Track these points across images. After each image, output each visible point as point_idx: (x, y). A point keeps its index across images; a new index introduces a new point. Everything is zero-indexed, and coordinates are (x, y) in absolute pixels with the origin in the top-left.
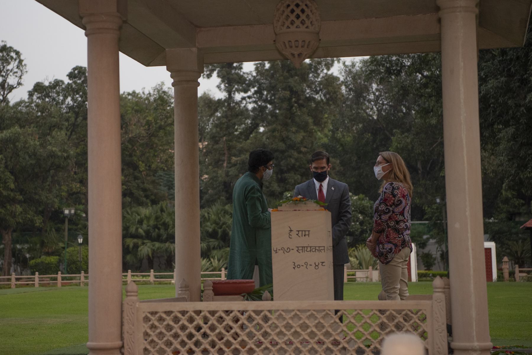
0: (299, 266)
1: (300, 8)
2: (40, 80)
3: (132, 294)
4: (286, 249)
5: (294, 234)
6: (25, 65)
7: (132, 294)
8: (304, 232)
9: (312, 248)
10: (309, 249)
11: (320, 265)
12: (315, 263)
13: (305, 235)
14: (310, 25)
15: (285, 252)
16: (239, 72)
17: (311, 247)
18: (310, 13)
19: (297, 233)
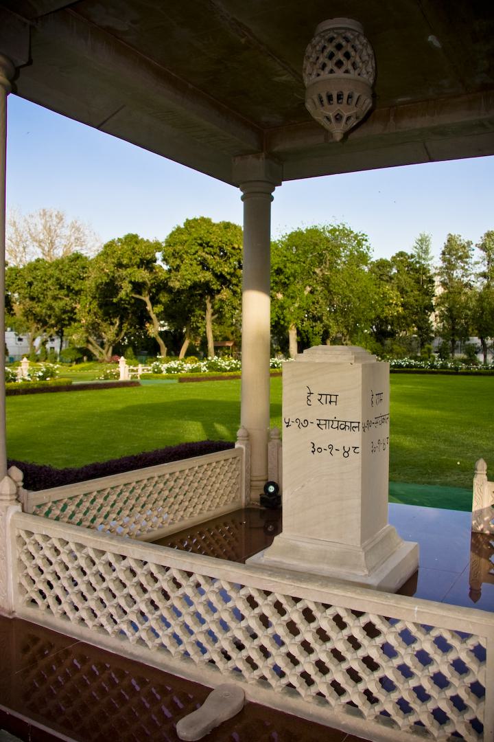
1: (343, 51)
2: (139, 235)
4: (302, 421)
5: (314, 398)
6: (421, 235)
8: (328, 397)
9: (340, 423)
10: (335, 425)
11: (351, 452)
13: (330, 402)
14: (350, 67)
17: (338, 421)
18: (358, 59)
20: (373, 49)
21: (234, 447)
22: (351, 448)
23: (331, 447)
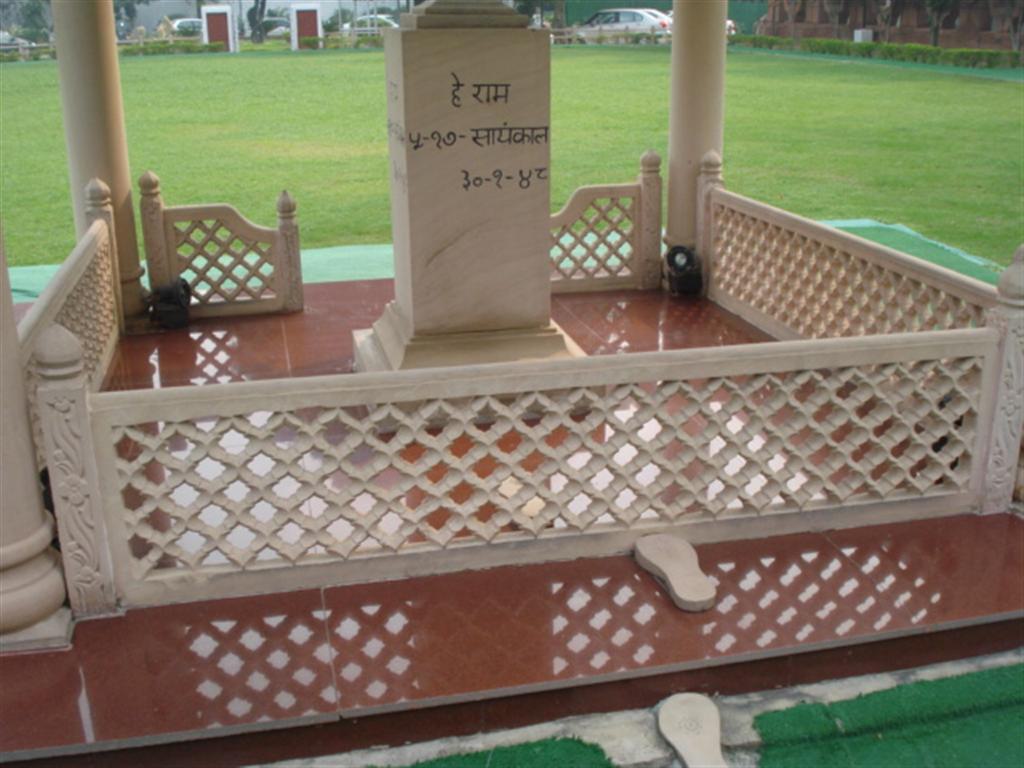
11: (534, 179)
15: (442, 144)
19: (475, 90)
22: (533, 171)
23: (498, 174)
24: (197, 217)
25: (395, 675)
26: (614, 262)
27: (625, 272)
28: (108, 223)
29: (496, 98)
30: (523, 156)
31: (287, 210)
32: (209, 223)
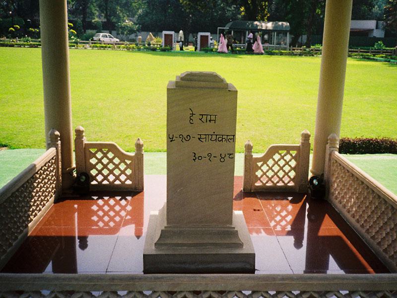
0: (200, 158)
3: (203, 84)
5: (196, 118)
7: (203, 84)
10: (214, 137)
11: (227, 158)
12: (221, 155)
16: (125, 23)
17: (217, 135)
19: (201, 117)
20: (264, 30)
21: (254, 273)
22: (226, 154)
23: (210, 155)
24: (100, 147)
25: (294, 237)
26: (286, 180)
27: (291, 184)
28: (57, 149)
29: (210, 121)
30: (218, 148)
31: (139, 147)
32: (105, 150)
